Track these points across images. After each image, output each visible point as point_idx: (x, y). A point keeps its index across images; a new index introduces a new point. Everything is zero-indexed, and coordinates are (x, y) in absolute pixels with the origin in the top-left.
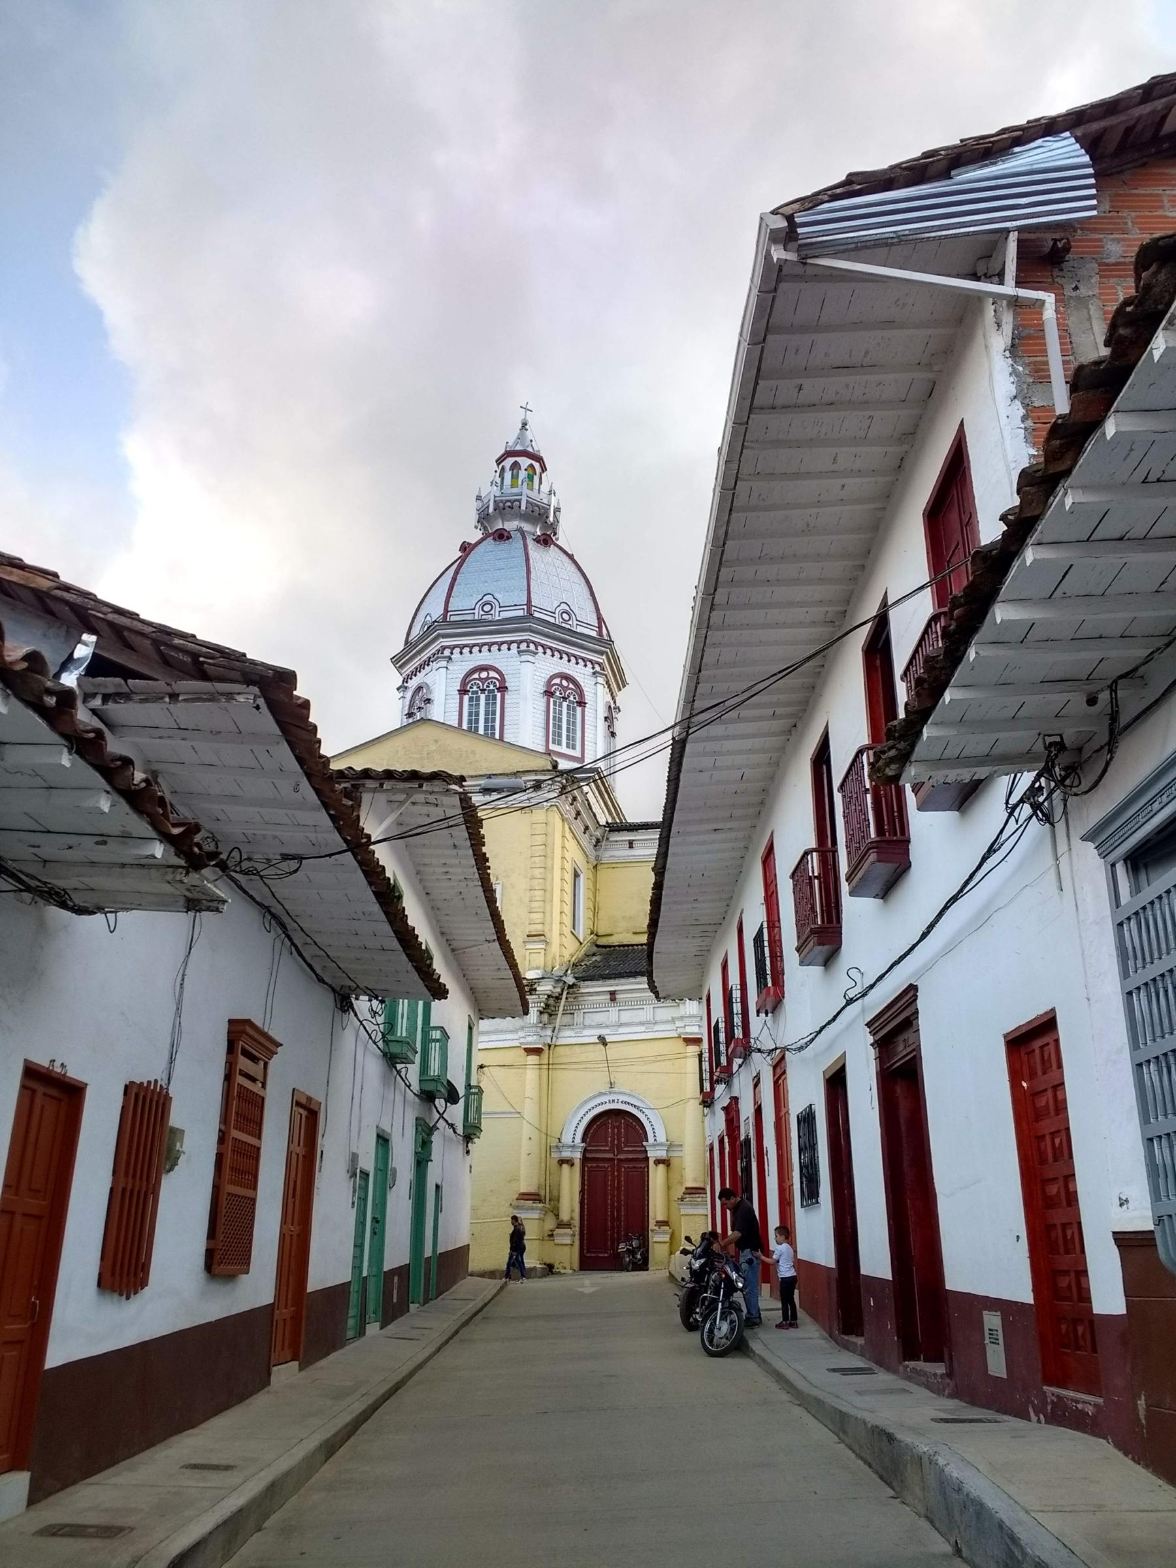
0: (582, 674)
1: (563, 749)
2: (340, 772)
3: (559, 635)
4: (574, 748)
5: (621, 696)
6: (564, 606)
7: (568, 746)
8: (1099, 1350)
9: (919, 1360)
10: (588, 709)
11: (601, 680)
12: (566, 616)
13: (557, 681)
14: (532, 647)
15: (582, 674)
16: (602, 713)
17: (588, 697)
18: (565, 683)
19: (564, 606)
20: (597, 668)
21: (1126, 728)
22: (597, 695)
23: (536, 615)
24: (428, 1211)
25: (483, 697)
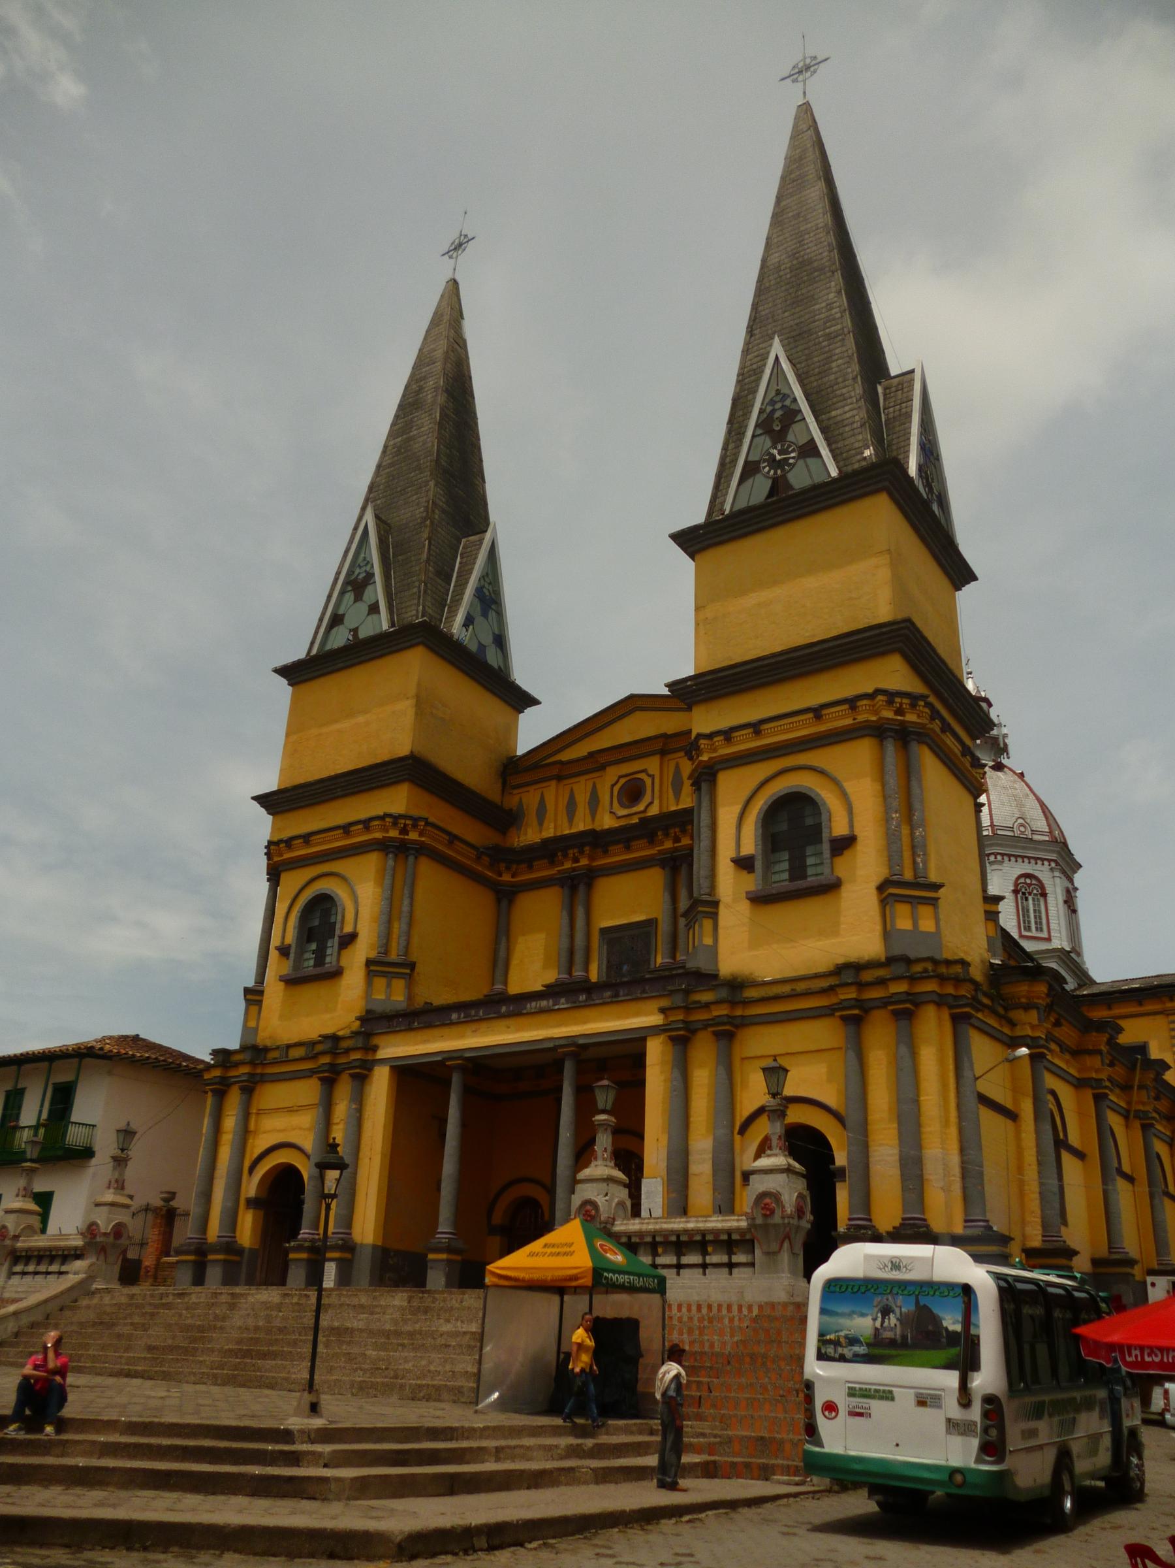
0: (1042, 872)
1: (1034, 933)
2: (593, 1141)
3: (1016, 844)
4: (1041, 930)
5: (1078, 878)
6: (1020, 821)
7: (1037, 929)
8: (747, 1134)
9: (237, 1285)
10: (1050, 899)
11: (1057, 874)
12: (1022, 829)
13: (1022, 880)
14: (999, 858)
15: (1042, 872)
16: (1061, 897)
17: (1049, 889)
18: (1028, 881)
19: (1020, 821)
20: (1053, 865)
21: (528, 1014)
22: (1055, 887)
23: (999, 832)
24: (287, 1469)
25: (1030, 898)
